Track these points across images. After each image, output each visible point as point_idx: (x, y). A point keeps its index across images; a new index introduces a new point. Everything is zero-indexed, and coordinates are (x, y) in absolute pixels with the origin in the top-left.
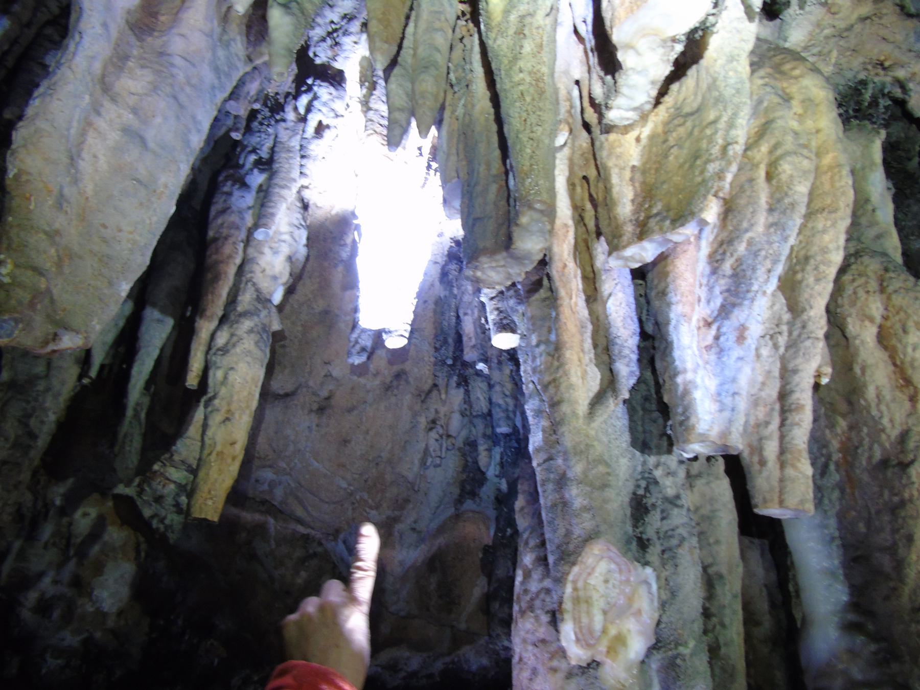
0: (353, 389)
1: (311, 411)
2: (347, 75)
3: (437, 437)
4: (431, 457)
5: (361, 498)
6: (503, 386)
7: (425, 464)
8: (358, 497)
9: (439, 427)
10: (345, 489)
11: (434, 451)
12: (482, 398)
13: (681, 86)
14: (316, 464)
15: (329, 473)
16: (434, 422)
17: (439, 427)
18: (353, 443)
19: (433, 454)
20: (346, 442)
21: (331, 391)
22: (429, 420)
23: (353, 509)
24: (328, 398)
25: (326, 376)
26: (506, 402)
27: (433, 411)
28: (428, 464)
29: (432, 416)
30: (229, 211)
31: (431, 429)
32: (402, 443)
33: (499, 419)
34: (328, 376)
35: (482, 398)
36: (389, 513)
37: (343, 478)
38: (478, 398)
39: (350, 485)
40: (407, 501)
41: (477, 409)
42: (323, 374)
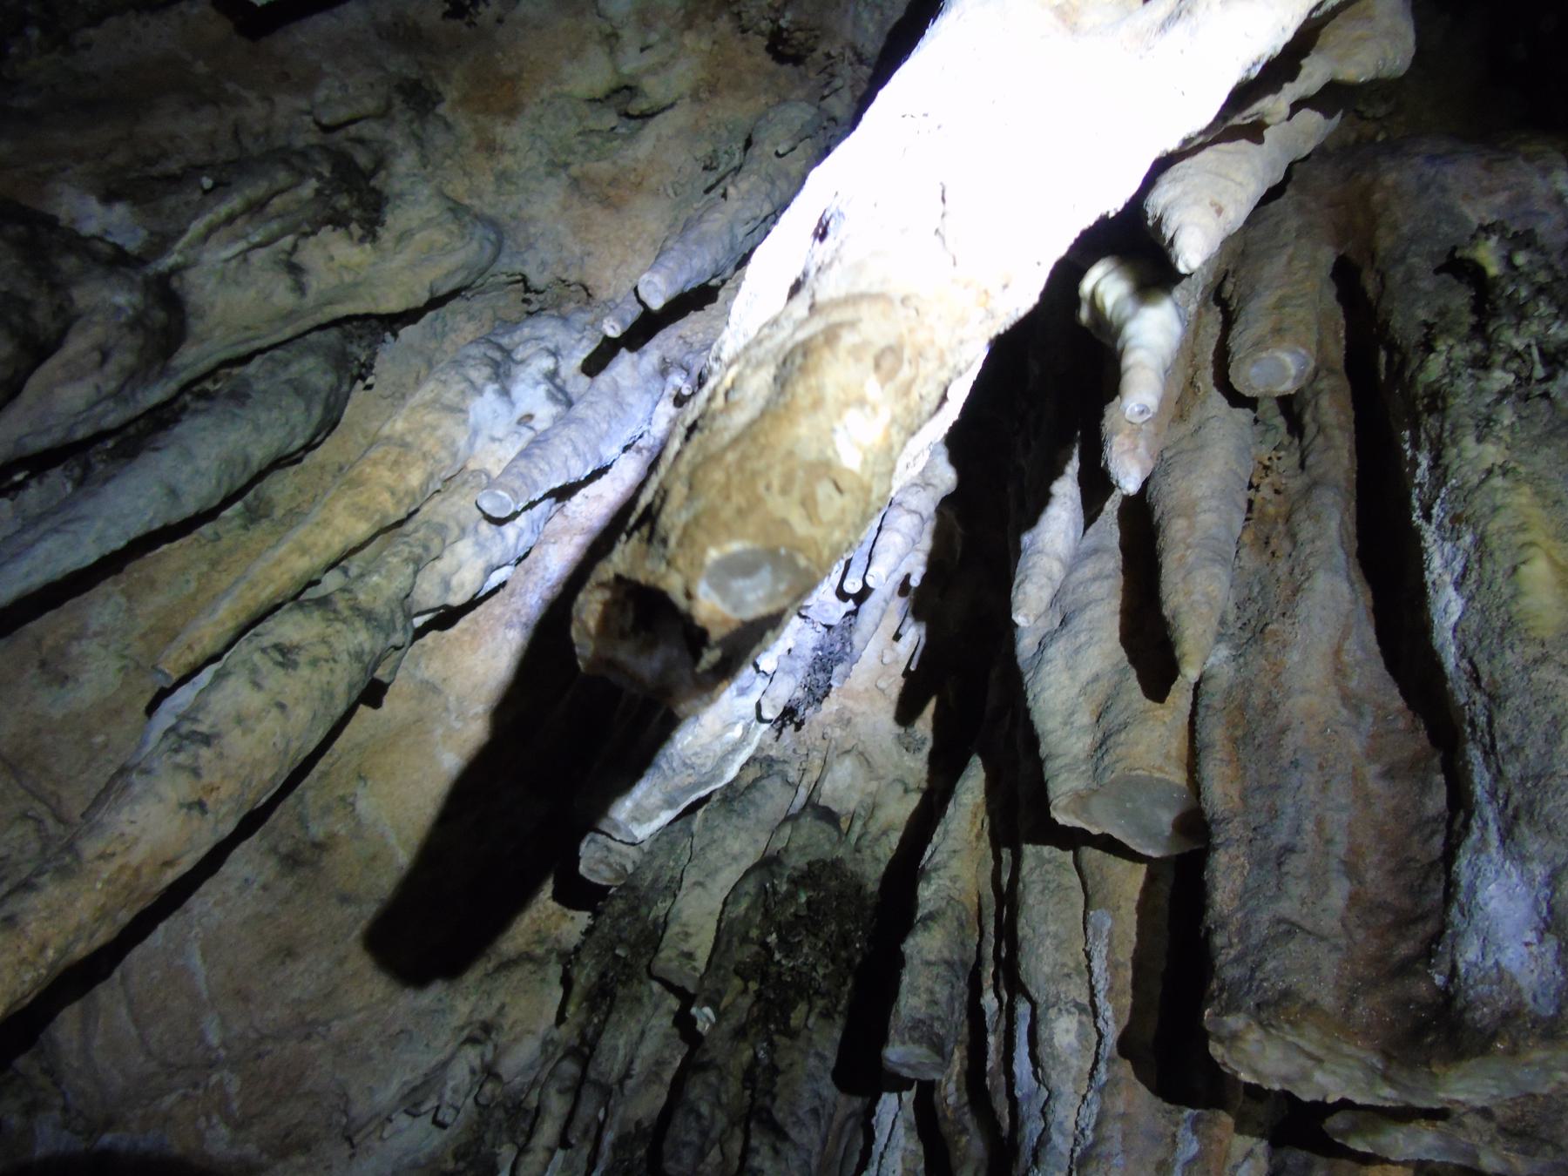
0: (374, 858)
1: (274, 850)
2: (580, 363)
3: (477, 1063)
4: (441, 1097)
5: (220, 1084)
6: (722, 1079)
7: (417, 1105)
8: (215, 1078)
9: (490, 1047)
10: (209, 1048)
11: (455, 1091)
12: (621, 1053)
13: (151, 521)
14: (197, 960)
15: (205, 995)
16: (487, 1028)
17: (490, 1047)
18: (302, 966)
19: (448, 1095)
20: (289, 953)
21: (332, 835)
22: (477, 1017)
23: (185, 1097)
24: (320, 846)
25: (342, 799)
26: (713, 1116)
27: (496, 1003)
28: (424, 1108)
29: (487, 1013)
30: (462, 416)
31: (472, 1040)
32: (396, 1028)
33: (686, 1144)
34: (348, 803)
35: (621, 1053)
36: (251, 1149)
37: (224, 1024)
38: (615, 1049)
39: (224, 1044)
40: (305, 1146)
41: (602, 1068)
42: (341, 792)
